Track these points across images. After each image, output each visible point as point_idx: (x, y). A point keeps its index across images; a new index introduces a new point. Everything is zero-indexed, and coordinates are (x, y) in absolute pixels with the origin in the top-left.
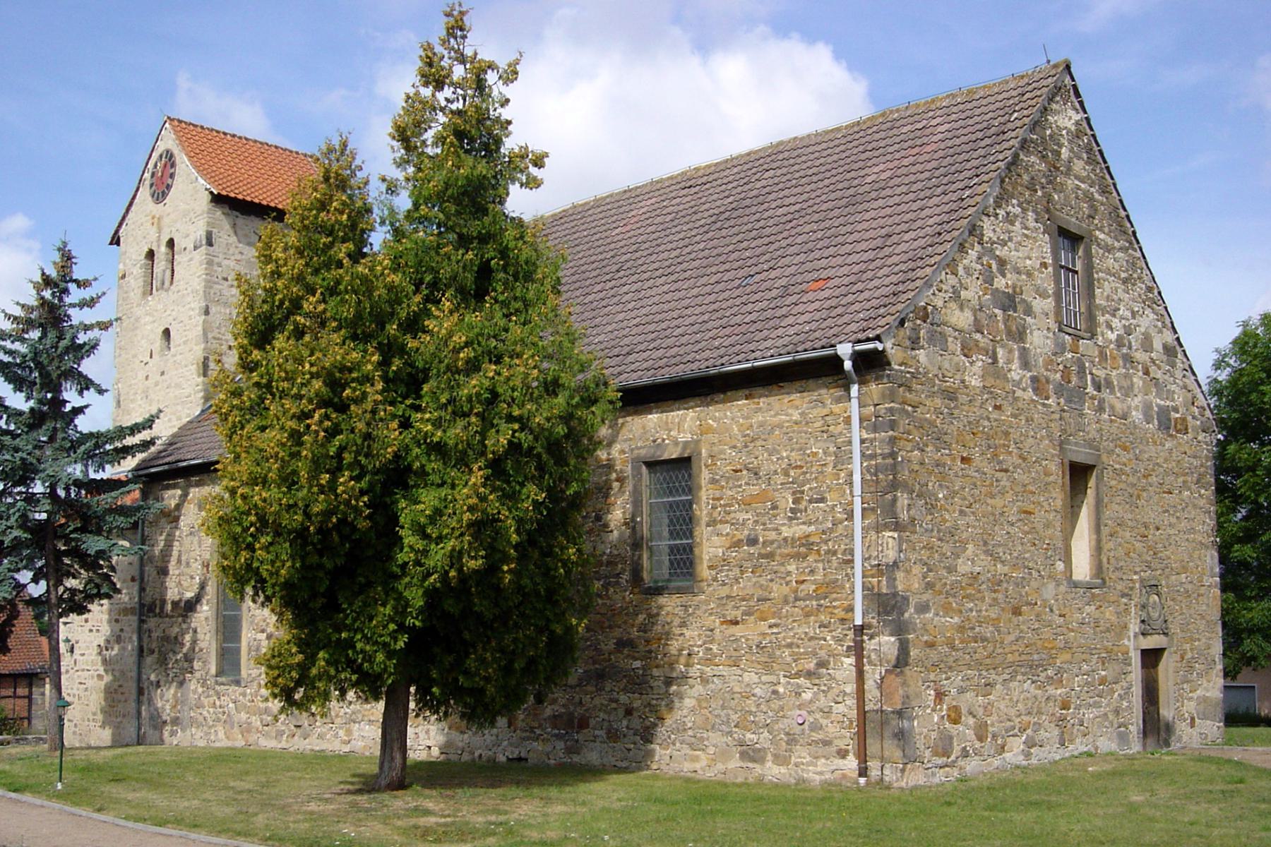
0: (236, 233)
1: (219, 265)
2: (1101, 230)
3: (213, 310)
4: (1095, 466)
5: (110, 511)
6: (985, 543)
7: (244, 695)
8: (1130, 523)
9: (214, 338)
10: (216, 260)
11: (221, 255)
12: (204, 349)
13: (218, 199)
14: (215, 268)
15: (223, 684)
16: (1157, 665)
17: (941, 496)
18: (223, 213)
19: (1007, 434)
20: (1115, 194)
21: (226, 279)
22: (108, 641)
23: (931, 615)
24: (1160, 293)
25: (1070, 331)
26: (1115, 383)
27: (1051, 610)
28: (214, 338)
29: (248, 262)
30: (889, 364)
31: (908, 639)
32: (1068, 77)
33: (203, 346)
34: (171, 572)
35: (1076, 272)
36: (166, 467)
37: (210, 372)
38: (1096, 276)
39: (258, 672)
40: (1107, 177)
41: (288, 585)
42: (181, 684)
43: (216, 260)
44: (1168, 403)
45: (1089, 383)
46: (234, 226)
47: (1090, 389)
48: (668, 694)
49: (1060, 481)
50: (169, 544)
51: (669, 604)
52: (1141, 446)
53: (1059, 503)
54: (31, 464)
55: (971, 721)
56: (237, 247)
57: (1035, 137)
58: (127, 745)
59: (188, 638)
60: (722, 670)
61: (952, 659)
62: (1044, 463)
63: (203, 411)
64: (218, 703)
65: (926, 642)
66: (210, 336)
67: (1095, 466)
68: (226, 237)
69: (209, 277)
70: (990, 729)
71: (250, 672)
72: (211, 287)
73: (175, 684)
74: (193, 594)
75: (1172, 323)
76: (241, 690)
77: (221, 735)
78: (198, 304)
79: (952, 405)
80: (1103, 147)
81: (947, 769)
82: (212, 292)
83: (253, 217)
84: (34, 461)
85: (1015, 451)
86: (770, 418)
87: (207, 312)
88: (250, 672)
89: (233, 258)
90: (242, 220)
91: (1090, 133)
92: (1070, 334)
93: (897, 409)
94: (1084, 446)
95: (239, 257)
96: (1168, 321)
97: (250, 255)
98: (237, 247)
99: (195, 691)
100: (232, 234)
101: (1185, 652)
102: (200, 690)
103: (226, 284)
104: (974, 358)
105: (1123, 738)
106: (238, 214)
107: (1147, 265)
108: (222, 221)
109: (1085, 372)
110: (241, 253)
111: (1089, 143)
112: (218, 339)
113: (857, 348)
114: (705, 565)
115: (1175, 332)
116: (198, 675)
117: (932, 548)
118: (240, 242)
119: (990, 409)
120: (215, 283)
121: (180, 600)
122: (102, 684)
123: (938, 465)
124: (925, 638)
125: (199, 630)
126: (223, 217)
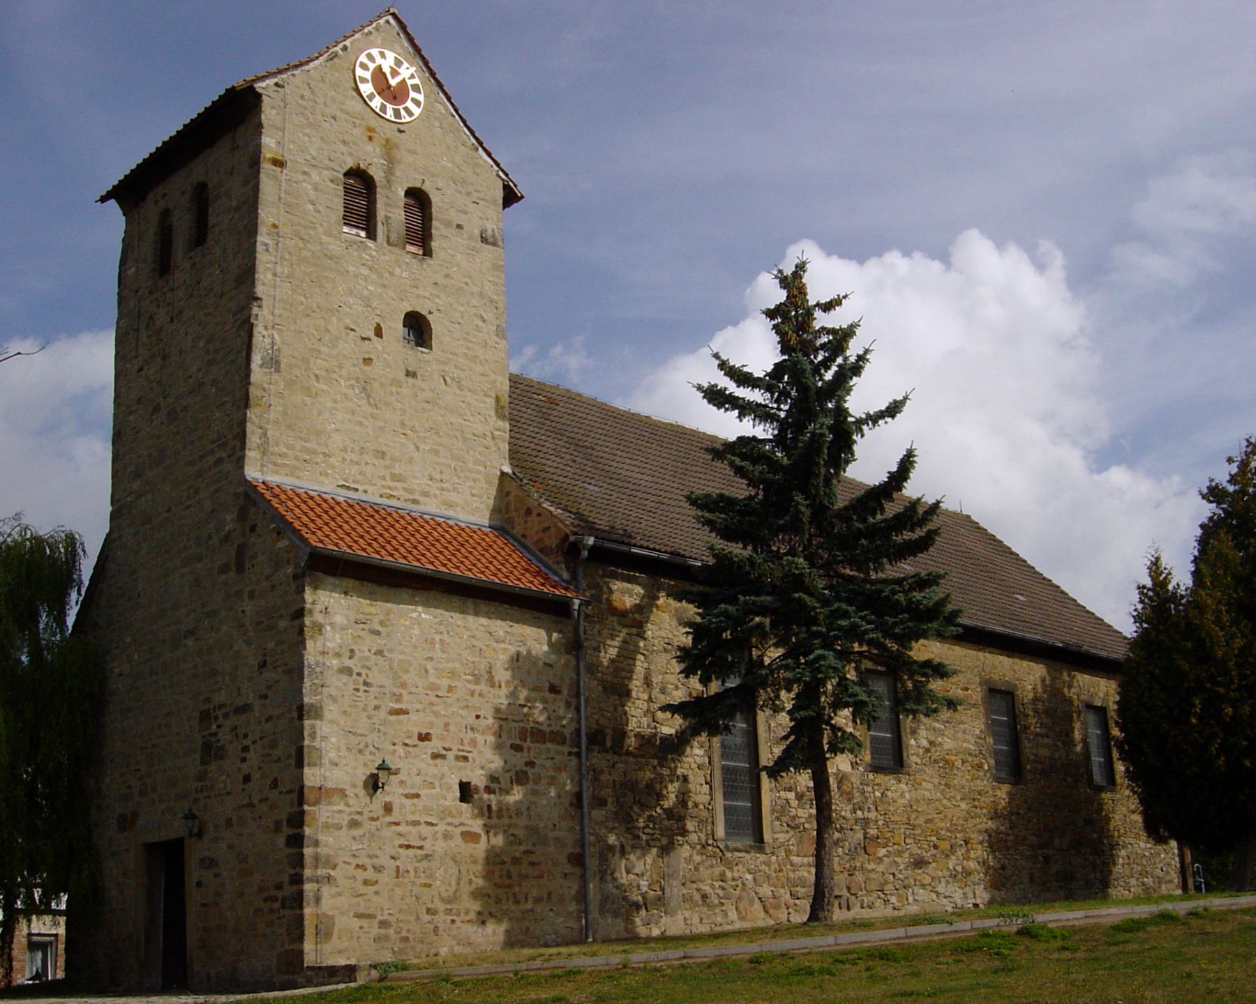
5: (563, 580)
7: (768, 864)
15: (738, 850)
22: (493, 778)
34: (634, 694)
36: (653, 554)
39: (788, 836)
41: (321, 634)
42: (666, 850)
48: (1112, 855)
50: (628, 654)
51: (1106, 796)
54: (804, 371)
58: (546, 945)
59: (673, 788)
60: (1131, 841)
64: (729, 874)
71: (776, 836)
73: (654, 851)
74: (673, 731)
76: (762, 857)
77: (733, 915)
84: (808, 367)
88: (776, 836)
99: (688, 860)
102: (697, 858)
116: (693, 838)
121: (655, 735)
122: (480, 849)
125: (691, 778)
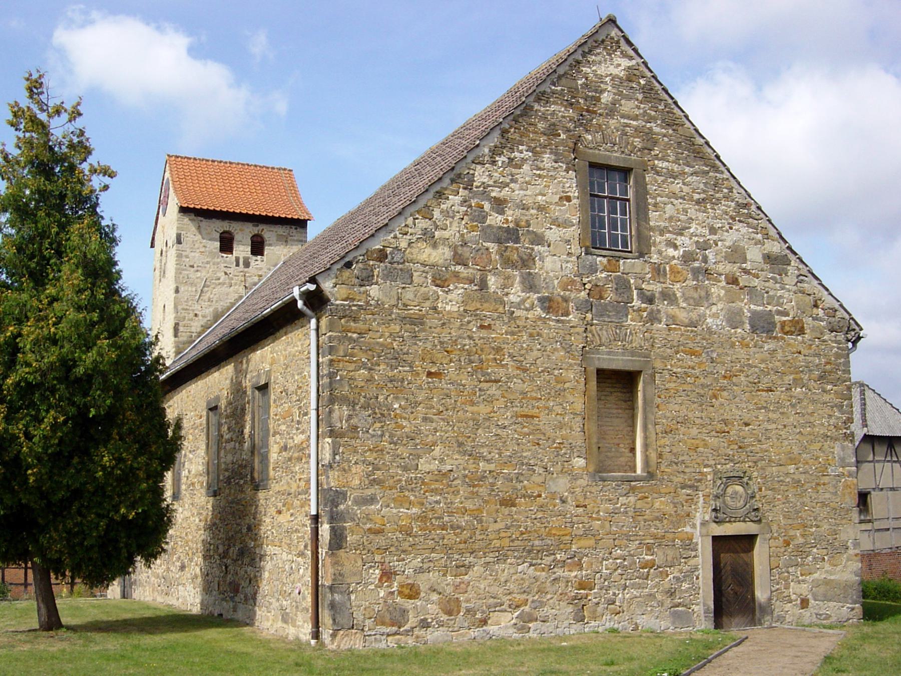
0: (200, 233)
1: (187, 257)
2: (663, 159)
3: (182, 289)
4: (641, 371)
6: (460, 444)
8: (698, 421)
9: (183, 309)
10: (184, 253)
11: (188, 250)
12: (175, 318)
13: (184, 210)
14: (184, 259)
16: (752, 549)
17: (396, 406)
18: (190, 220)
19: (498, 350)
20: (688, 124)
21: (192, 266)
23: (378, 507)
24: (759, 208)
25: (604, 253)
26: (679, 295)
27: (563, 501)
28: (183, 309)
29: (211, 252)
30: (329, 300)
31: (345, 528)
32: (616, 30)
33: (174, 315)
35: (628, 200)
37: (179, 334)
38: (650, 201)
40: (676, 110)
43: (184, 253)
44: (769, 308)
45: (635, 297)
46: (199, 228)
47: (636, 303)
49: (582, 386)
52: (720, 350)
53: (579, 406)
55: (435, 597)
56: (201, 243)
57: (559, 88)
61: (408, 544)
62: (556, 372)
63: (174, 362)
65: (369, 529)
66: (180, 307)
67: (641, 371)
68: (192, 236)
69: (178, 266)
70: (464, 605)
72: (181, 273)
75: (779, 234)
78: (173, 286)
79: (417, 329)
80: (666, 85)
81: (398, 637)
82: (181, 276)
83: (214, 220)
85: (511, 363)
86: (292, 350)
87: (177, 291)
89: (198, 251)
90: (205, 223)
91: (649, 74)
92: (604, 256)
93: (335, 337)
94: (623, 354)
95: (203, 250)
96: (772, 232)
97: (212, 247)
98: (201, 243)
100: (197, 234)
101: (793, 538)
103: (192, 269)
104: (451, 287)
105: (681, 617)
106: (202, 219)
107: (739, 183)
108: (189, 225)
109: (630, 288)
110: (205, 247)
111: (649, 82)
112: (186, 309)
113: (302, 289)
114: (271, 468)
115: (786, 242)
117: (382, 450)
118: (203, 238)
119: (474, 330)
120: (184, 270)
123: (391, 381)
124: (368, 526)
126: (189, 222)
